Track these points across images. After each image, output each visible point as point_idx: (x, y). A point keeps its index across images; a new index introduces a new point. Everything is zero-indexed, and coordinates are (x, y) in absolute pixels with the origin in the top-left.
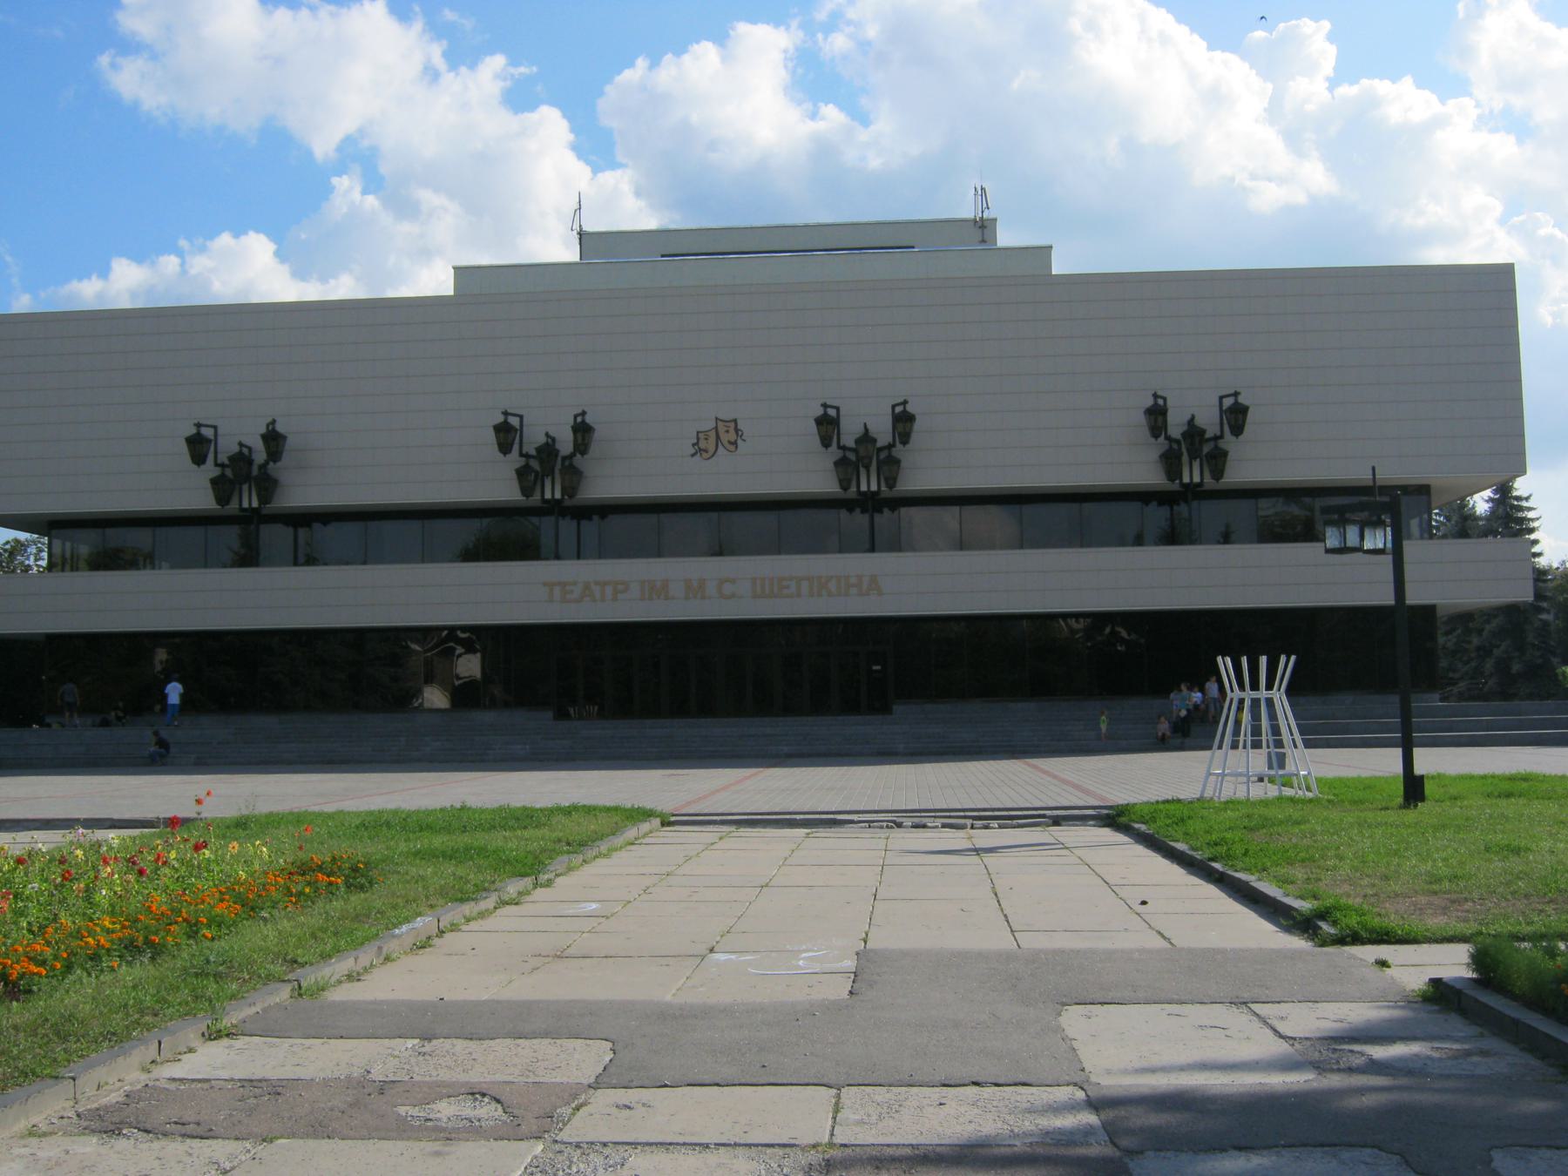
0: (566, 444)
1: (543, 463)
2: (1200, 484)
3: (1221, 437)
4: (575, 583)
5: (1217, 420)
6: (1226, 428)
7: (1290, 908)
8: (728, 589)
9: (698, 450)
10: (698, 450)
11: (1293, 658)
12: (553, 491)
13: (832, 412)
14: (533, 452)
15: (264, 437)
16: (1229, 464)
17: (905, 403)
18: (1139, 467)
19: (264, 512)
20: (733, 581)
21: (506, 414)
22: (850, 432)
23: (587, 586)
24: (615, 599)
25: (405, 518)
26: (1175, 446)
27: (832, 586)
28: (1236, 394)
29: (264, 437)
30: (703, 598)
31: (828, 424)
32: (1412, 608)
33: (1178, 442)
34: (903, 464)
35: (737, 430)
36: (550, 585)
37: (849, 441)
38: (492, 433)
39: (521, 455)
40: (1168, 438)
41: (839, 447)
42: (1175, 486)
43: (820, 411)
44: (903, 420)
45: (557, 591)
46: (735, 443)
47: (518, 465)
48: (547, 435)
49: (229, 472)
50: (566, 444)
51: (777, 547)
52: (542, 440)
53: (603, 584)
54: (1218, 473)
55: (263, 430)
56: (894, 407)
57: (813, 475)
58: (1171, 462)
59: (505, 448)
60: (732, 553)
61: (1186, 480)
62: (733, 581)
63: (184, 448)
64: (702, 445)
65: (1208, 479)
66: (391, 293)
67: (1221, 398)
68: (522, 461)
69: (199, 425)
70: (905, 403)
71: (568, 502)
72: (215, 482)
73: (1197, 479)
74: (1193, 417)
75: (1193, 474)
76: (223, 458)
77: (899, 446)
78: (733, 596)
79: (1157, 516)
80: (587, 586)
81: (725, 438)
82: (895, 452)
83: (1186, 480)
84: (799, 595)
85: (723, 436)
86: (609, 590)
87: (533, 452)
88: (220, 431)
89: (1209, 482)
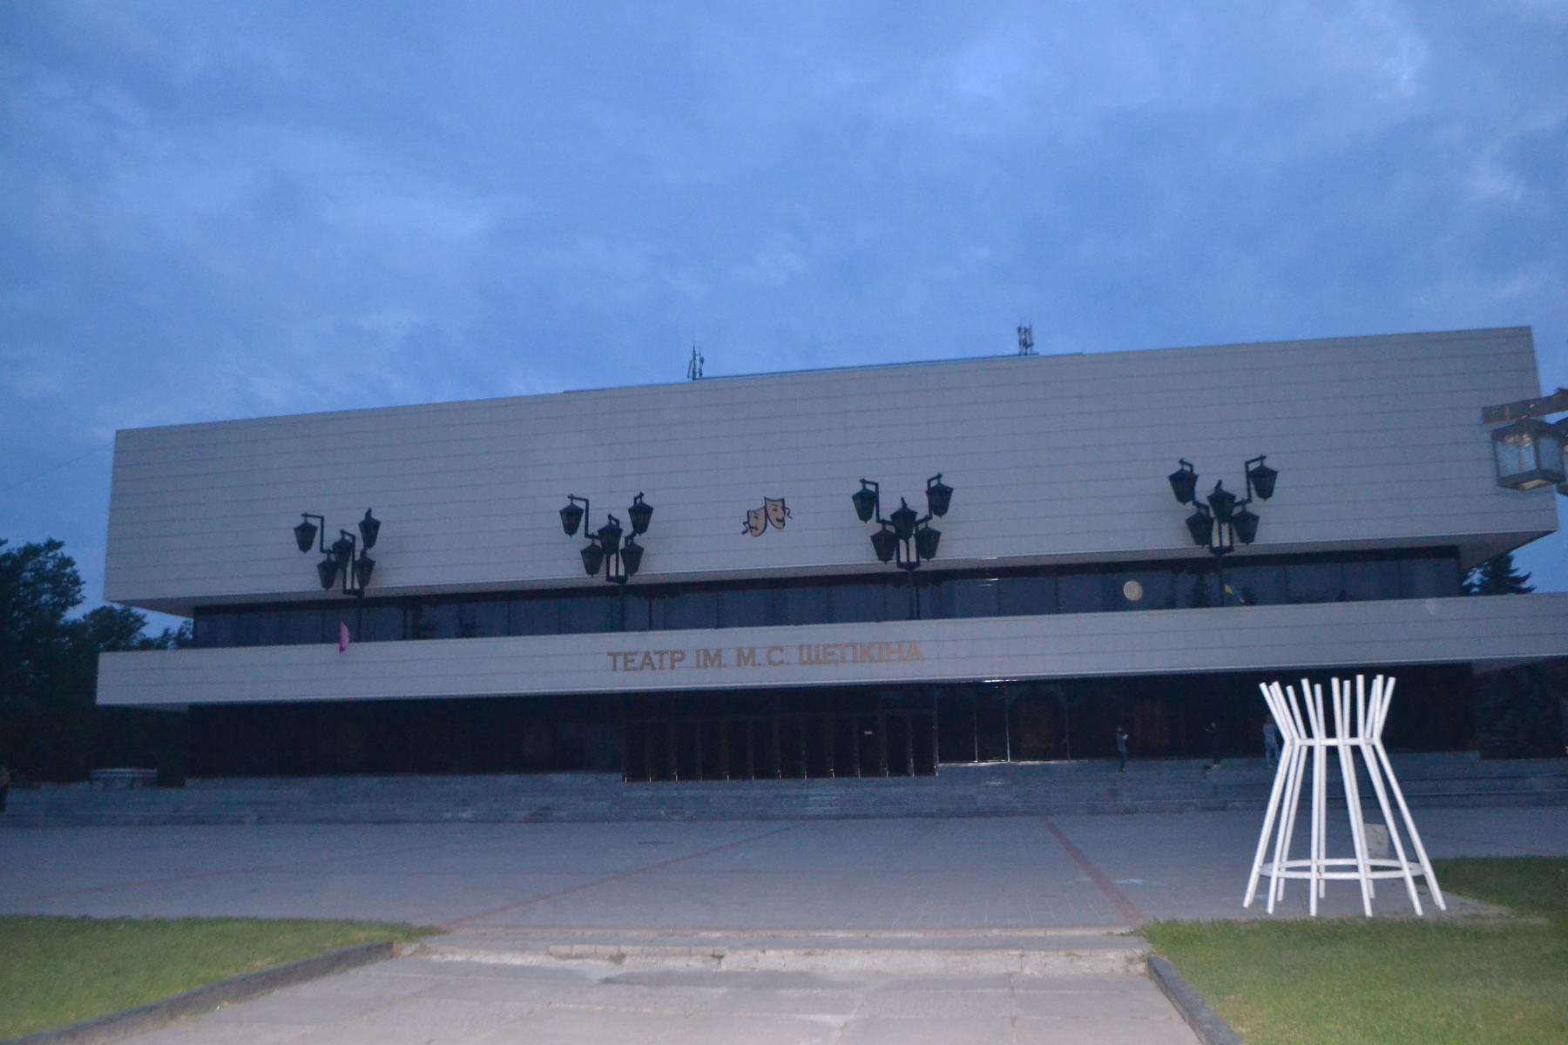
0: (922, 509)
1: (348, 557)
2: (1230, 549)
3: (1249, 500)
4: (635, 653)
5: (1244, 485)
6: (1253, 492)
7: (450, 964)
8: (776, 656)
9: (750, 528)
10: (750, 528)
11: (1392, 681)
12: (616, 567)
13: (871, 488)
14: (888, 518)
15: (631, 511)
16: (940, 544)
17: (939, 477)
18: (1164, 534)
19: (367, 594)
20: (781, 649)
21: (572, 497)
22: (888, 506)
23: (647, 655)
24: (673, 667)
25: (1010, 573)
26: (1203, 511)
27: (875, 652)
28: (1262, 458)
29: (631, 511)
30: (720, 666)
31: (866, 502)
32: (109, 709)
33: (1206, 508)
34: (376, 566)
35: (784, 508)
36: (614, 655)
37: (886, 515)
38: (1168, 483)
39: (587, 535)
40: (1197, 504)
41: (878, 520)
42: (1202, 552)
43: (859, 487)
44: (370, 527)
45: (620, 660)
46: (782, 521)
47: (583, 547)
48: (610, 517)
49: (598, 543)
50: (922, 509)
51: (828, 617)
52: (605, 522)
53: (661, 653)
54: (1247, 536)
55: (363, 518)
56: (1247, 463)
57: (850, 549)
58: (1199, 527)
59: (570, 529)
60: (1354, 599)
61: (1216, 543)
62: (781, 649)
63: (558, 522)
64: (753, 523)
65: (1238, 544)
66: (437, 400)
67: (1247, 463)
68: (879, 527)
69: (306, 515)
70: (939, 477)
71: (926, 565)
72: (875, 538)
73: (1226, 543)
74: (1220, 483)
75: (1221, 536)
76: (593, 530)
77: (935, 517)
78: (782, 662)
79: (1186, 582)
80: (647, 655)
81: (772, 515)
82: (1250, 508)
83: (1216, 543)
84: (844, 661)
85: (769, 516)
86: (667, 659)
87: (888, 518)
88: (326, 523)
89: (1241, 549)
